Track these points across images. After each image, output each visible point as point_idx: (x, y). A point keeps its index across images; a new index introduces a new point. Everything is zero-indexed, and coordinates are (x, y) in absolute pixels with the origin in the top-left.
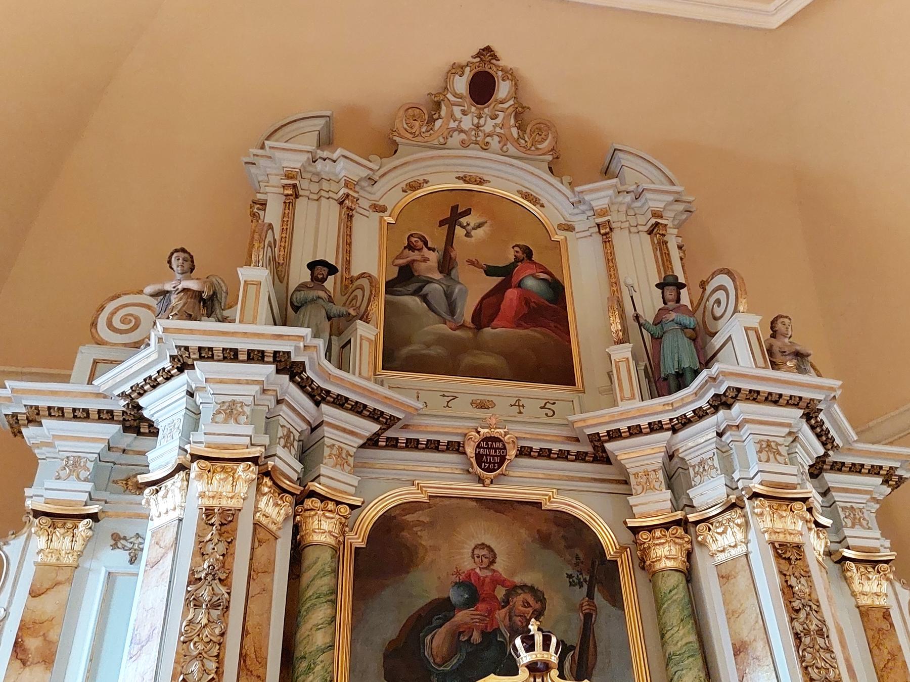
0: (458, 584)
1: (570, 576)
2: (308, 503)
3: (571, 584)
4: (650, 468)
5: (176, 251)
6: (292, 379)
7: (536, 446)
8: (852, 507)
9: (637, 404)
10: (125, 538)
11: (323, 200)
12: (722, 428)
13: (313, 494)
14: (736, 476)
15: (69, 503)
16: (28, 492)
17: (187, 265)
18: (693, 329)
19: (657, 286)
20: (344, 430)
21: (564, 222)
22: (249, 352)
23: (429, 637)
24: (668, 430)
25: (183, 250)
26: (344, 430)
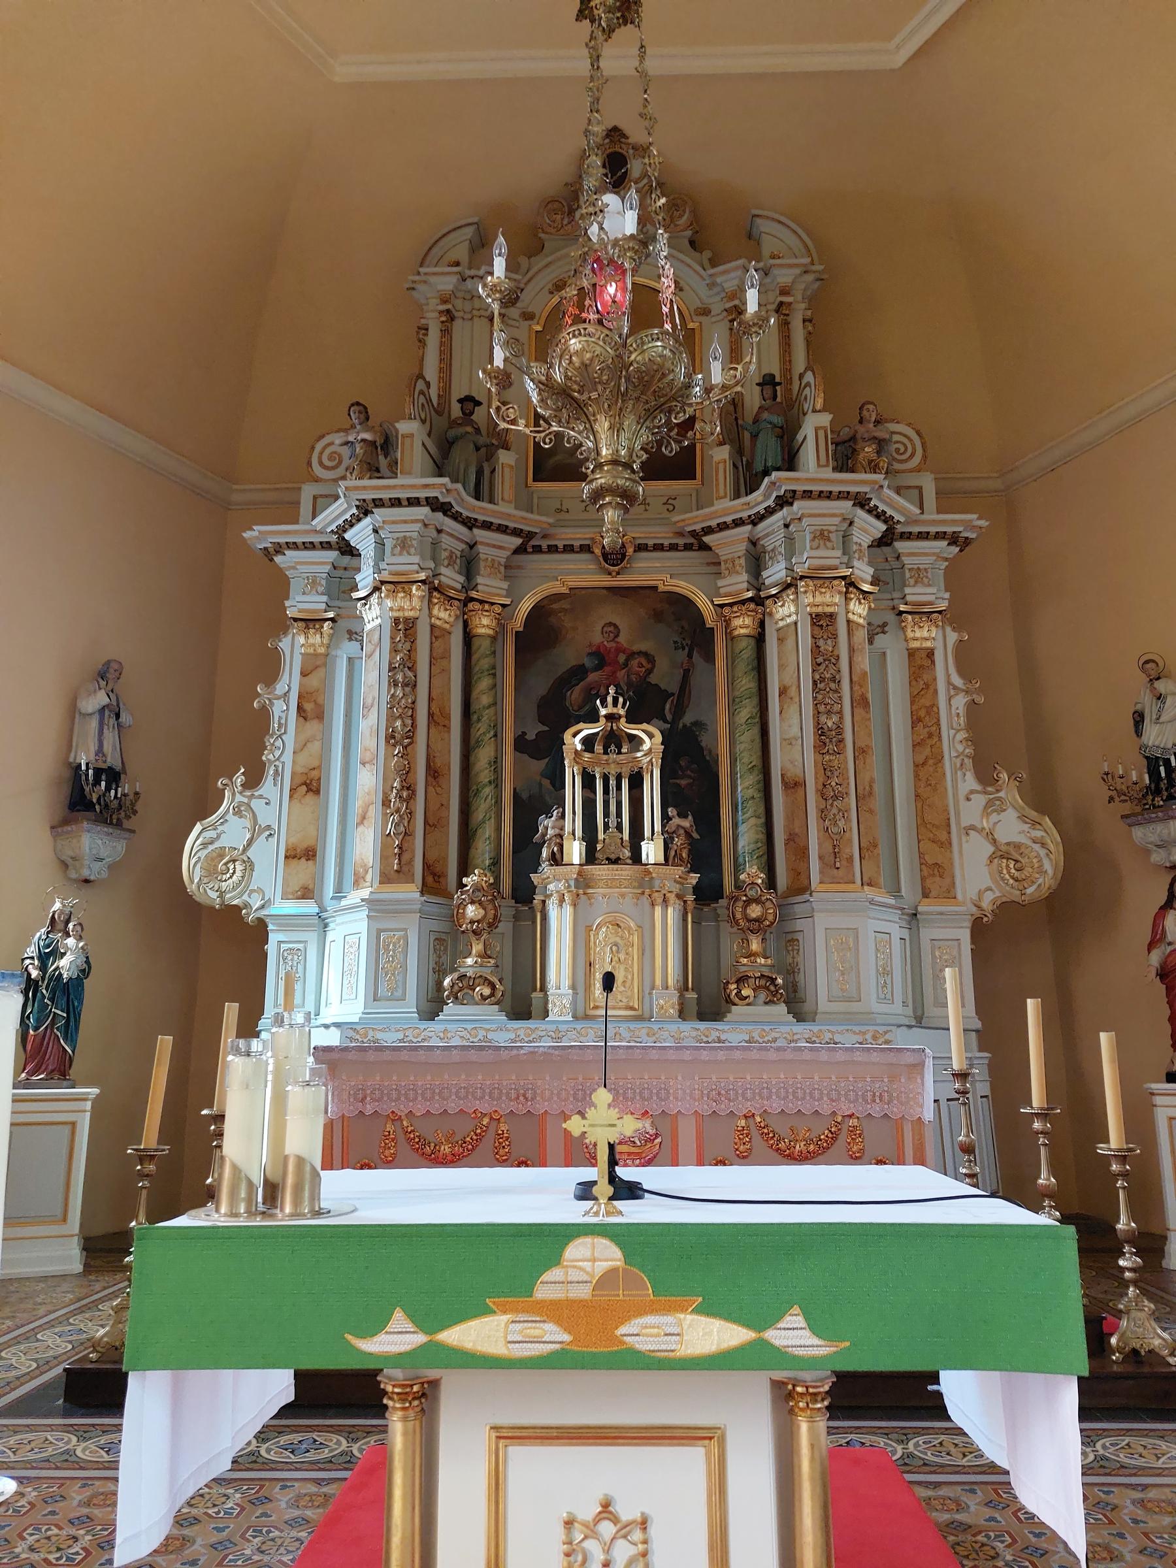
0: (589, 654)
1: (675, 642)
2: (471, 605)
3: (676, 649)
4: (736, 555)
5: (353, 405)
6: (445, 514)
7: (651, 543)
8: (919, 568)
9: (727, 503)
10: (356, 633)
11: (476, 319)
12: (788, 520)
13: (473, 599)
14: (794, 561)
15: (315, 611)
16: (287, 603)
17: (362, 416)
18: (781, 428)
19: (758, 384)
20: (494, 546)
21: (700, 305)
22: (408, 499)
23: (569, 692)
24: (748, 524)
25: (358, 404)
26: (494, 546)
